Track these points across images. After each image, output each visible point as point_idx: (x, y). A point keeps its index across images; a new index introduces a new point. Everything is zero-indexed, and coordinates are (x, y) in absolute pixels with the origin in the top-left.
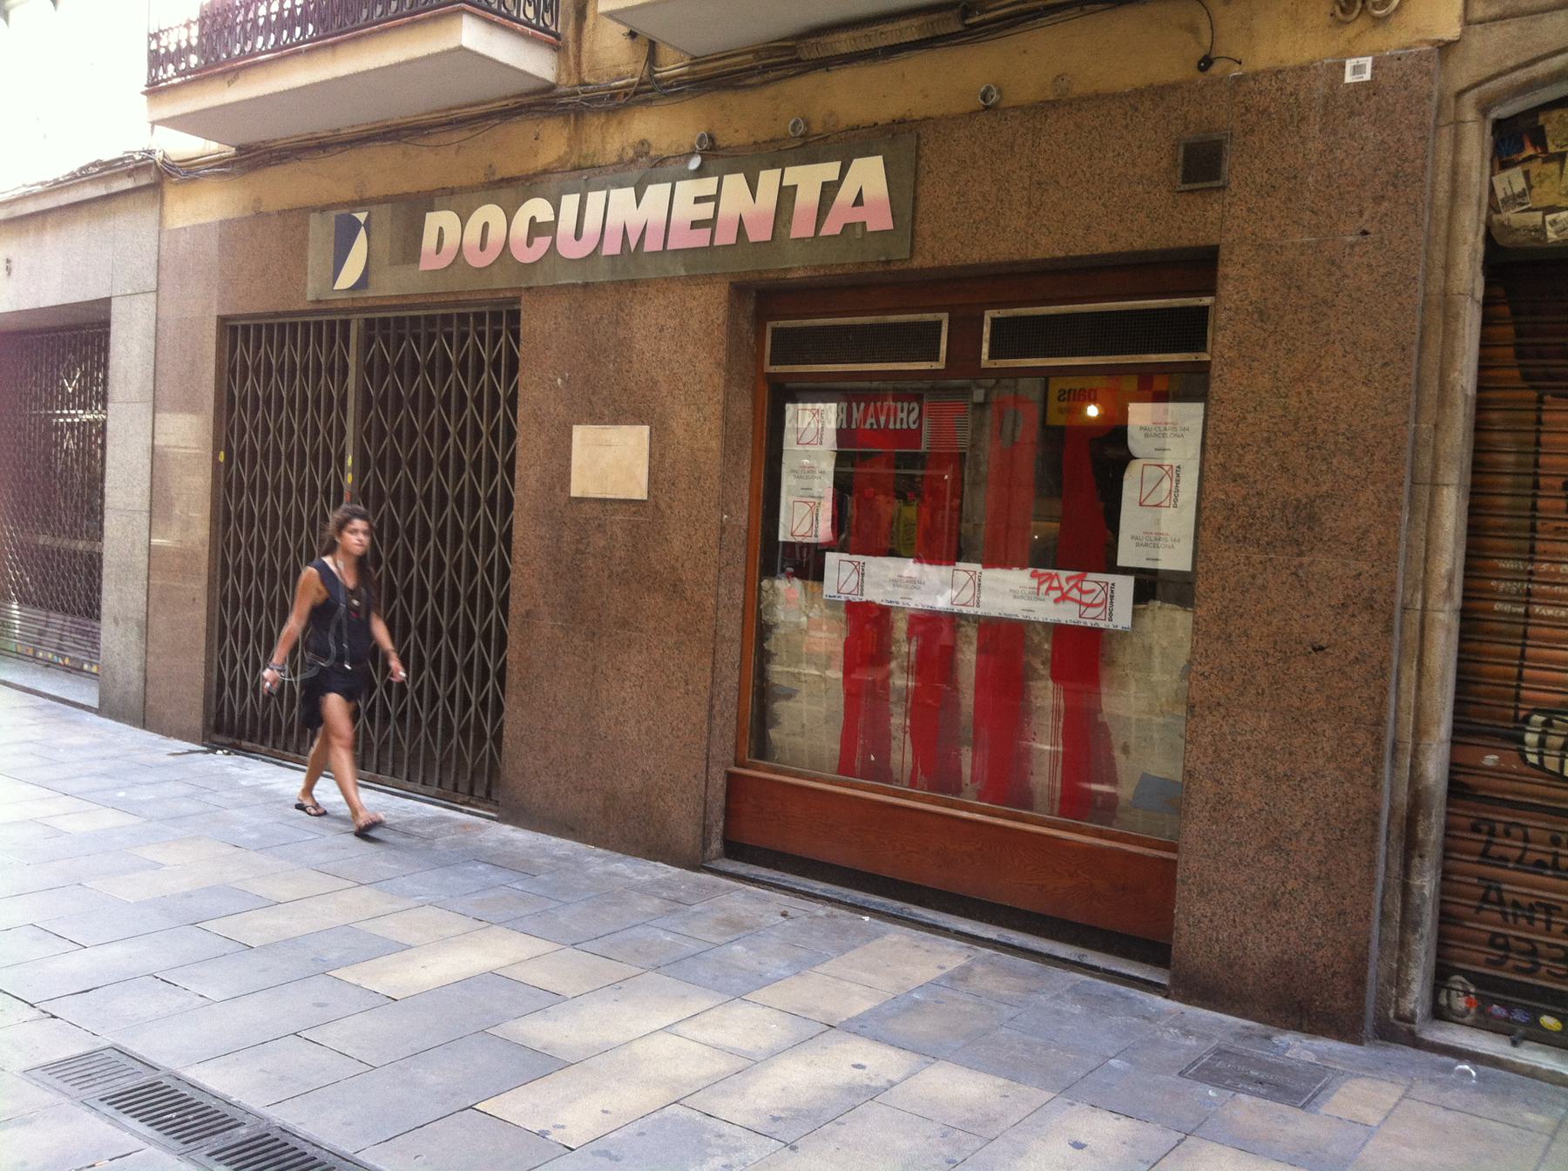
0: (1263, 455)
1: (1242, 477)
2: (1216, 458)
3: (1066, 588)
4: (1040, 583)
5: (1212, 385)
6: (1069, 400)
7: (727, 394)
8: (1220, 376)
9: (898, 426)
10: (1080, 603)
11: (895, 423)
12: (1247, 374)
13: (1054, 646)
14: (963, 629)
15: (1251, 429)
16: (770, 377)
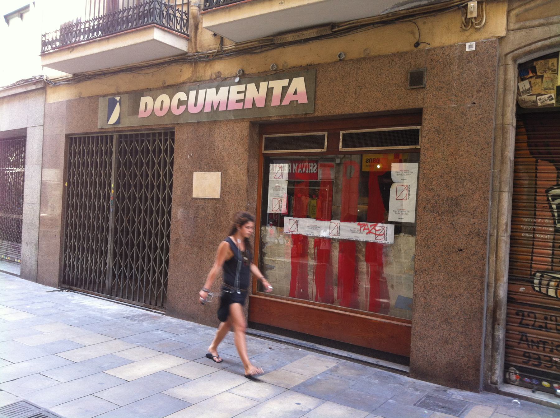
1: (432, 189)
2: (423, 182)
3: (370, 229)
4: (361, 227)
5: (421, 157)
8: (424, 153)
9: (309, 172)
10: (375, 234)
14: (334, 244)
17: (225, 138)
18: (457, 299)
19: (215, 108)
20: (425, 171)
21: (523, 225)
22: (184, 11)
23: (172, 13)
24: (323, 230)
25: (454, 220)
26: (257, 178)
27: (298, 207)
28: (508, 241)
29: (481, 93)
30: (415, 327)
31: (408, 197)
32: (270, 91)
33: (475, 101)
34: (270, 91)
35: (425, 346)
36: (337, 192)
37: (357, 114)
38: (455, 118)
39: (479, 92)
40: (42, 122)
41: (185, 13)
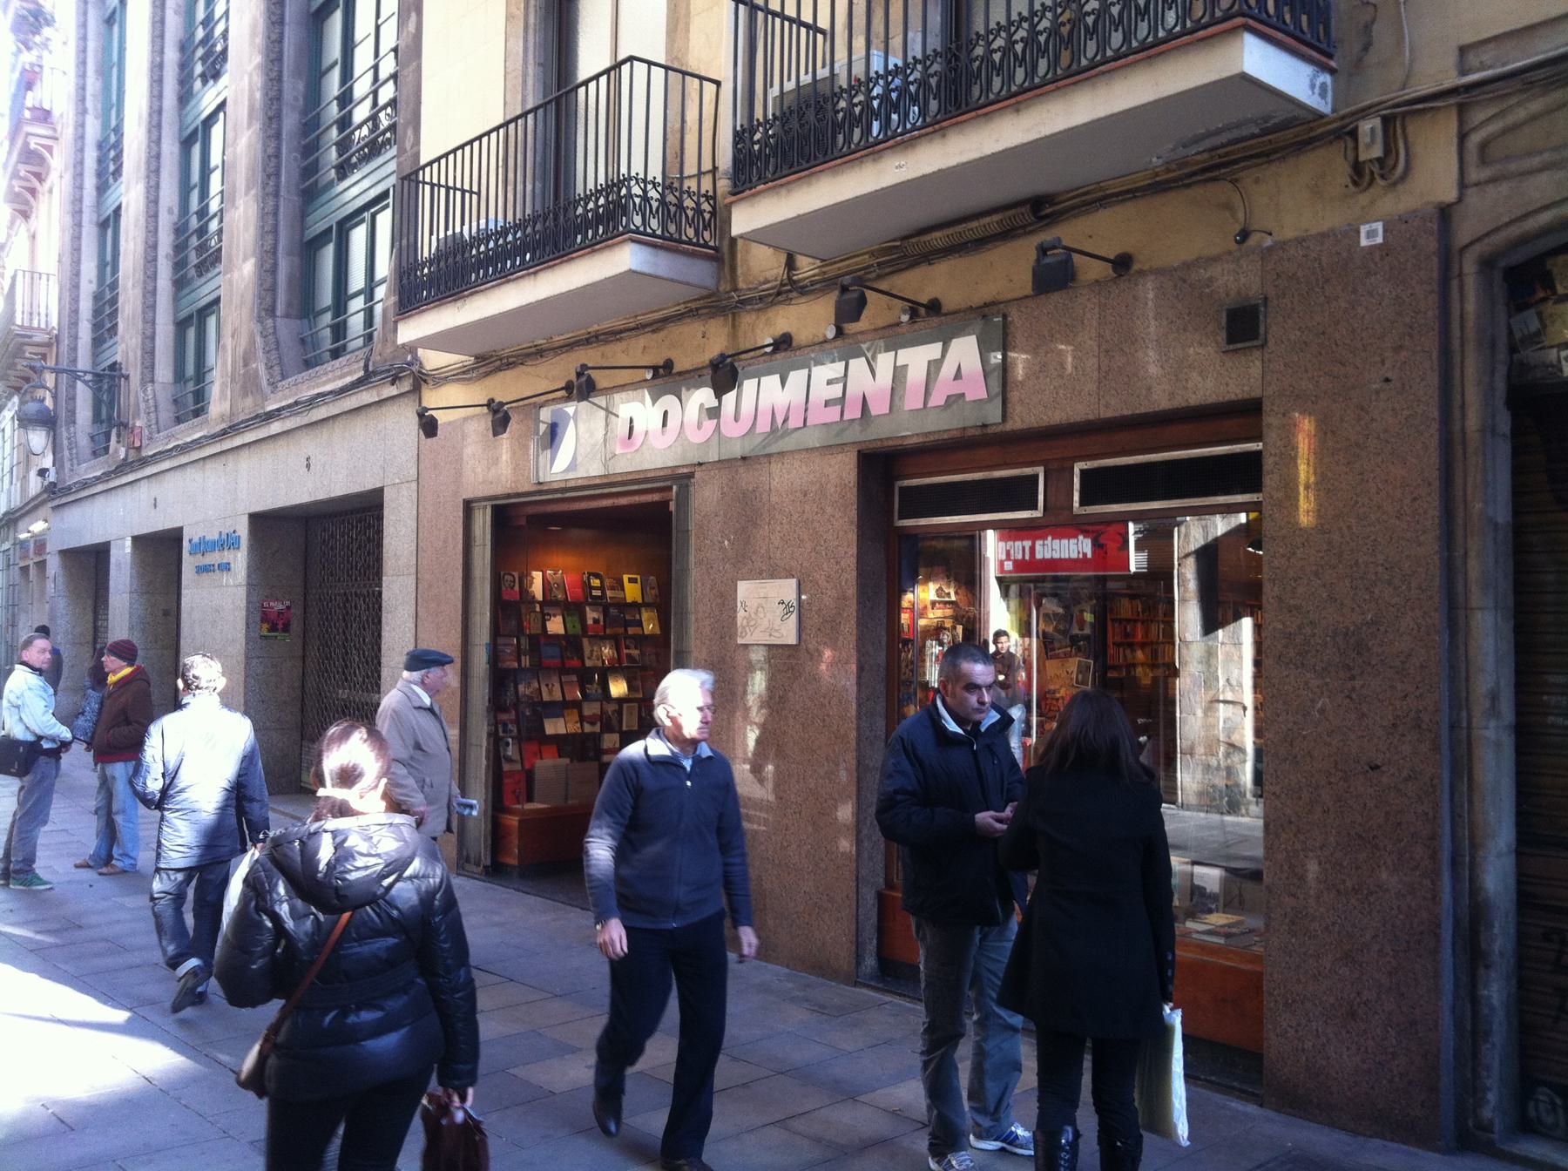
1: (1298, 608)
17: (805, 495)
18: (1372, 899)
19: (779, 421)
21: (1548, 694)
22: (703, 191)
23: (674, 201)
24: (710, 719)
25: (1353, 689)
26: (885, 591)
28: (1508, 742)
29: (1404, 353)
30: (1271, 974)
32: (899, 373)
33: (1389, 375)
34: (899, 373)
35: (1299, 1025)
37: (1140, 415)
38: (1342, 420)
39: (1398, 349)
40: (414, 471)
41: (704, 196)
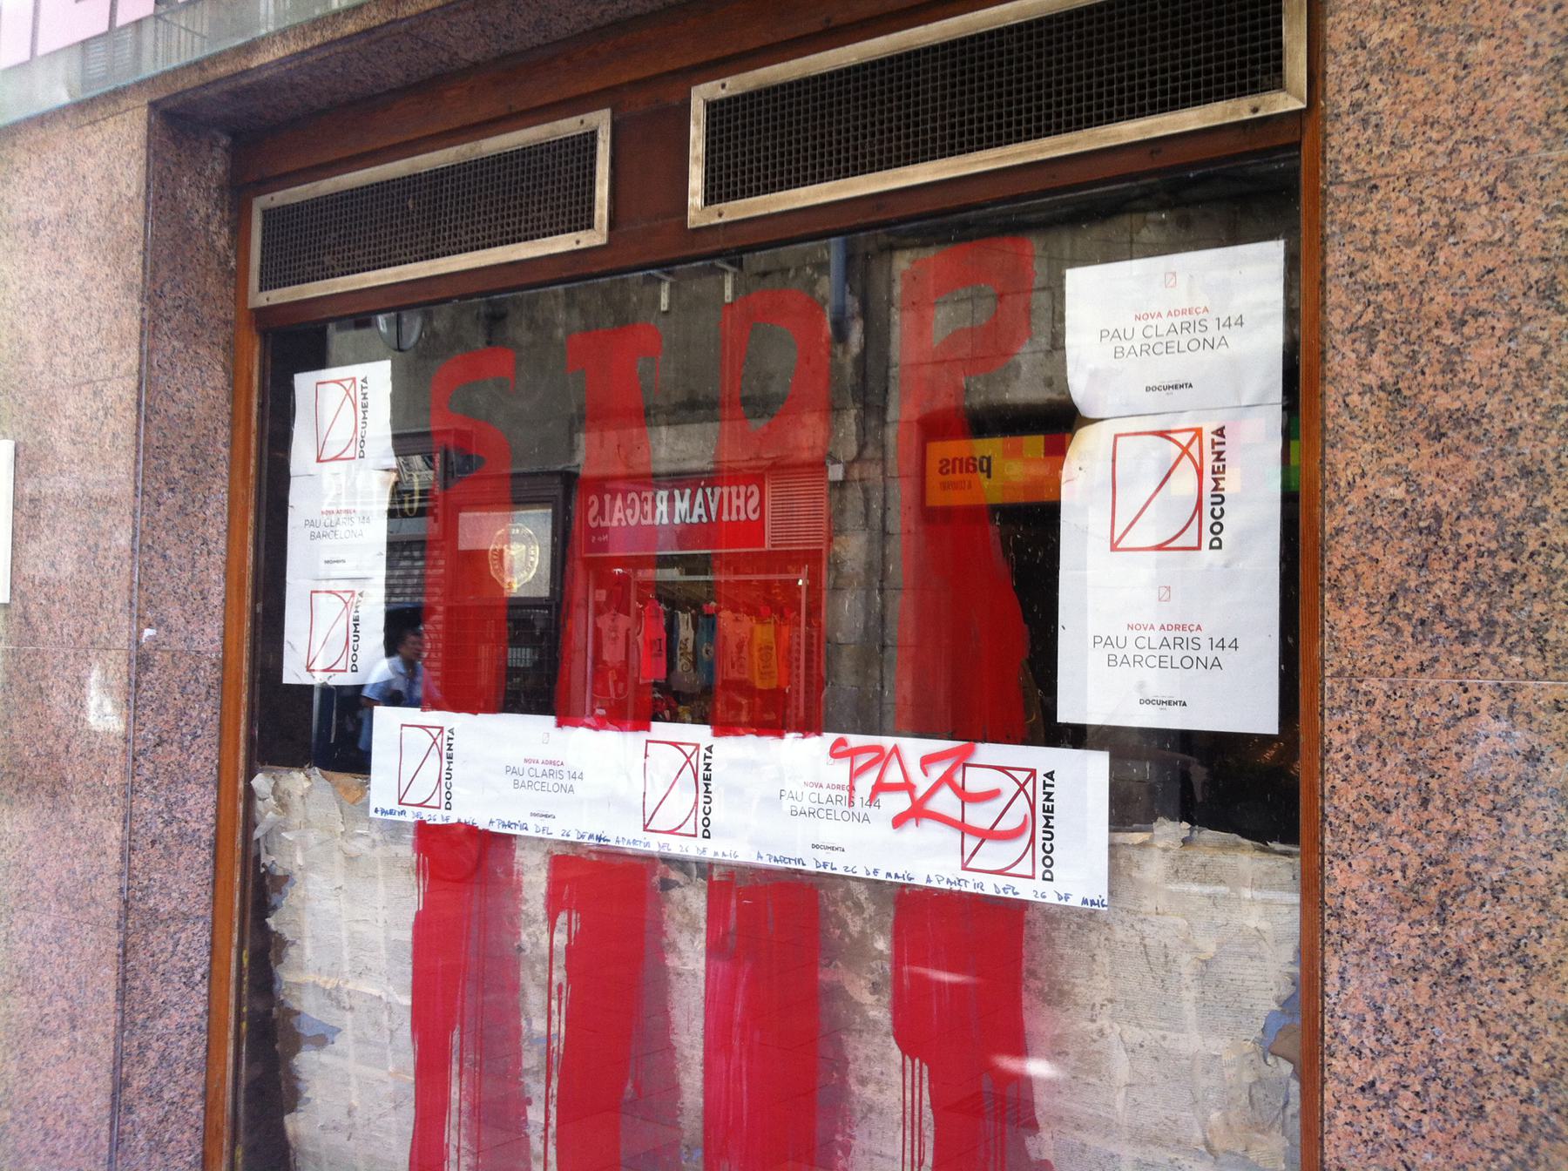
0: (1533, 340)
1: (1459, 419)
2: (1363, 366)
3: (923, 785)
4: (855, 774)
5: (1335, 141)
6: (954, 472)
7: (146, 355)
8: (1356, 106)
9: (734, 518)
10: (963, 828)
11: (730, 514)
12: (1451, 86)
13: (897, 944)
14: (675, 893)
15: (1482, 260)
16: (264, 319)
20: (1379, 265)
27: (707, 652)
31: (1208, 521)
36: (836, 589)
